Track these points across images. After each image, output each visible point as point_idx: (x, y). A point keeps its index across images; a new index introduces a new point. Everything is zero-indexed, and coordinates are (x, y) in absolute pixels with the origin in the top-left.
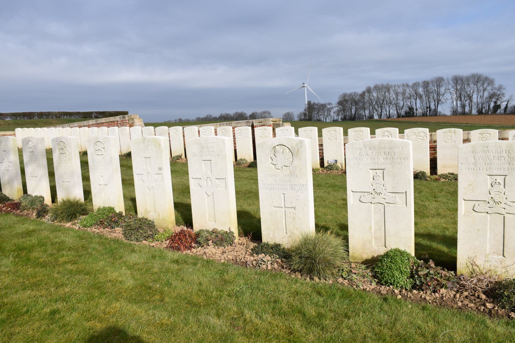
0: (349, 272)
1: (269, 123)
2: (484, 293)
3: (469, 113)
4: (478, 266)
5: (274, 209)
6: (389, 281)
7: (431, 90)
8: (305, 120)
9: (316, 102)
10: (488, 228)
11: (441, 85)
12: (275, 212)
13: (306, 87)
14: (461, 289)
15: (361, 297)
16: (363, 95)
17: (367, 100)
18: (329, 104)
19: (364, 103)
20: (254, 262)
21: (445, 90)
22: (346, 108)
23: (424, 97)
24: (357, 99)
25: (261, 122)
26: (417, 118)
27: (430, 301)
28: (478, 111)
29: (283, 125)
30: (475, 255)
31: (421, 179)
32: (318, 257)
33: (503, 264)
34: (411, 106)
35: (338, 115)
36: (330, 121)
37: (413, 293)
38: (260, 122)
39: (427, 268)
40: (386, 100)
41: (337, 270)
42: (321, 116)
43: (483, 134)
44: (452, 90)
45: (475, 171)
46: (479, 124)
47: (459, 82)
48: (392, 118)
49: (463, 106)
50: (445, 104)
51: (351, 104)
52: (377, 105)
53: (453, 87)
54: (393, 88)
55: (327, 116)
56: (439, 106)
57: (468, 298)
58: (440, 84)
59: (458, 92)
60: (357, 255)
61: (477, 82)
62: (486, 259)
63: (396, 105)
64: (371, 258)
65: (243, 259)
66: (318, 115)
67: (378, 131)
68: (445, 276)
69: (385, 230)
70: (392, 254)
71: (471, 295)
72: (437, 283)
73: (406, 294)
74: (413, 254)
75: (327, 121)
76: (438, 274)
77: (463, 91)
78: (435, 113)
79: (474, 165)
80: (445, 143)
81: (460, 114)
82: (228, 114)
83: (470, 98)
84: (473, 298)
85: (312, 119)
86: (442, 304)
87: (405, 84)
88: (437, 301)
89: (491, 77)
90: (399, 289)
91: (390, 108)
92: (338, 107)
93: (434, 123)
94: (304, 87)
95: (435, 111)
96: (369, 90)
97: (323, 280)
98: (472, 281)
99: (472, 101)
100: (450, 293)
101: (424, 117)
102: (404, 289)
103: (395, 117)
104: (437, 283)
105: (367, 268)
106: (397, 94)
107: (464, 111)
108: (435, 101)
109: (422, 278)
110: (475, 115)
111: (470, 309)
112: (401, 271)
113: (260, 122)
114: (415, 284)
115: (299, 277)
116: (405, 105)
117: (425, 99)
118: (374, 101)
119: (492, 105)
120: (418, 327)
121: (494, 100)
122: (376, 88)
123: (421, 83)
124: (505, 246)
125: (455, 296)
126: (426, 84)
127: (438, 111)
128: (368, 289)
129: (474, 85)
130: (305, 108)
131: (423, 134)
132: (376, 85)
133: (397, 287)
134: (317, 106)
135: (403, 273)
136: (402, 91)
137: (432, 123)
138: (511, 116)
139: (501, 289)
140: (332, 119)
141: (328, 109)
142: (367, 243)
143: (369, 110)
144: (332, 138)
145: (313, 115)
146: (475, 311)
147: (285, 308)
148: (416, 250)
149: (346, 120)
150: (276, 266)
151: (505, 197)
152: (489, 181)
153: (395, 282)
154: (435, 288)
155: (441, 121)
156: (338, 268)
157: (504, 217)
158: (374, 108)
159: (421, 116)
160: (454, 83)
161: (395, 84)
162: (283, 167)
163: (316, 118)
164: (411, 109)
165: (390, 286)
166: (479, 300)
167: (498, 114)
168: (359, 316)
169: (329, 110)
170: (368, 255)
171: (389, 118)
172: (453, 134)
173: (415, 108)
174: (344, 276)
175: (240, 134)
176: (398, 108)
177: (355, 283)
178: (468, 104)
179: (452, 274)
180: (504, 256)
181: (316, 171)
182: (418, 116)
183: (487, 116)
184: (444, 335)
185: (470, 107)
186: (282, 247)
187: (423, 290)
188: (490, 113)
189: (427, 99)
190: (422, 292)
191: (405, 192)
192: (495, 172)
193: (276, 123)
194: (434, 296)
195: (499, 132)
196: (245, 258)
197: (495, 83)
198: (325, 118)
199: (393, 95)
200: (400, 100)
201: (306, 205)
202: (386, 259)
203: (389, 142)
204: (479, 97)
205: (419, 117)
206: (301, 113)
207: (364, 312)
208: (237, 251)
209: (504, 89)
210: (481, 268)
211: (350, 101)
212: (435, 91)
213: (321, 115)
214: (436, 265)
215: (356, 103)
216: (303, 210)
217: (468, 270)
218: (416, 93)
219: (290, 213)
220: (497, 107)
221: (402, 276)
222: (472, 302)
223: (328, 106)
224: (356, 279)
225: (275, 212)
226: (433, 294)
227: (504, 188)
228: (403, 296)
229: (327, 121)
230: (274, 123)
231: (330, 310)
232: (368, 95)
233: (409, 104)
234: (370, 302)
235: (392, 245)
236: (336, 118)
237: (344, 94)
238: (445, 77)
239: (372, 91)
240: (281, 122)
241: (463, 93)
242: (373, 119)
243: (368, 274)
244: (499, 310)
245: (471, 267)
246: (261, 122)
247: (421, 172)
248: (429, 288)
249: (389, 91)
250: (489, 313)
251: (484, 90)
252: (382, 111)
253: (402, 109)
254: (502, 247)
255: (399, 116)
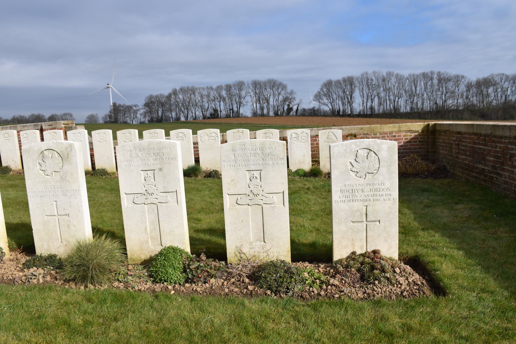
0: (125, 274)
1: (60, 126)
2: (248, 277)
3: (267, 114)
4: (244, 254)
5: (46, 218)
6: (163, 279)
7: (234, 93)
8: (110, 123)
9: (121, 104)
10: (250, 219)
11: (242, 89)
12: (48, 221)
13: (110, 88)
14: (229, 276)
15: (133, 298)
16: (169, 97)
17: (173, 102)
18: (135, 106)
19: (171, 105)
20: (23, 278)
21: (246, 93)
22: (153, 110)
23: (227, 99)
24: (163, 101)
25: (51, 125)
26: (221, 119)
27: (201, 292)
28: (274, 113)
29: (76, 128)
30: (241, 244)
31: (214, 177)
32: (91, 263)
33: (264, 249)
34: (216, 108)
35: (145, 117)
36: (136, 123)
37: (185, 286)
38: (49, 125)
39: (199, 261)
40: (192, 103)
41: (113, 274)
42: (127, 118)
43: (266, 134)
44: (252, 93)
45: (236, 167)
46: (275, 125)
47: (258, 86)
48: (198, 119)
49: (262, 109)
50: (246, 106)
51: (158, 106)
52: (184, 107)
53: (252, 91)
54: (198, 90)
55: (133, 118)
56: (241, 108)
57: (234, 284)
58: (241, 88)
59: (257, 95)
60: (135, 256)
61: (273, 87)
62: (251, 247)
63: (202, 107)
64: (149, 258)
65: (10, 276)
66: (124, 117)
67: (172, 133)
68: (215, 266)
69: (160, 229)
70: (165, 252)
71: (238, 281)
72: (207, 274)
73: (179, 289)
74: (188, 249)
75: (134, 123)
76: (208, 265)
77: (261, 95)
78: (238, 115)
79: (234, 162)
80: (124, 143)
81: (259, 116)
82: (23, 117)
83: (268, 101)
84: (238, 283)
85: (118, 122)
86: (211, 293)
87: (209, 86)
88: (207, 291)
89: (284, 83)
90: (173, 285)
91: (196, 110)
92: (144, 109)
93: (237, 124)
94: (108, 87)
95: (238, 113)
96: (175, 92)
97: (99, 286)
98: (238, 267)
99: (269, 104)
100: (219, 282)
101: (227, 119)
102: (178, 284)
103: (201, 118)
104: (207, 274)
105: (144, 268)
106: (202, 97)
107: (263, 112)
108: (237, 103)
109: (194, 272)
110: (273, 116)
111: (235, 293)
112: (174, 267)
113: (49, 125)
114: (188, 278)
115: (73, 286)
116: (209, 107)
117: (228, 102)
118: (180, 102)
119: (286, 107)
120: (183, 318)
121: (287, 103)
122: (182, 90)
123: (224, 86)
124: (265, 233)
125: (223, 283)
126: (228, 88)
127: (240, 113)
128: (143, 289)
129: (271, 89)
130: (109, 110)
131: (214, 135)
132: (182, 87)
133: (171, 282)
134: (123, 107)
135: (176, 269)
136: (206, 93)
137: (235, 124)
138: (301, 117)
139: (259, 271)
140: (139, 121)
141: (134, 111)
142: (144, 243)
143: (176, 112)
144: (127, 141)
145: (119, 117)
146: (239, 294)
147: (50, 321)
148: (191, 244)
149: (153, 122)
150: (48, 278)
151: (261, 189)
152: (248, 176)
153: (169, 278)
154: (206, 279)
155: (243, 123)
156: (115, 272)
157: (262, 207)
158: (180, 110)
159: (225, 118)
160: (254, 87)
161: (200, 86)
162: (53, 172)
163: (122, 121)
164: (216, 111)
165: (165, 283)
166: (243, 284)
167: (291, 116)
168: (128, 317)
169: (135, 112)
170: (145, 256)
171: (195, 119)
172: (241, 134)
173: (219, 110)
174: (120, 280)
175: (27, 139)
176: (203, 110)
177: (130, 285)
178: (266, 107)
179: (222, 264)
180: (265, 242)
181: (111, 174)
182: (222, 117)
183: (282, 117)
184: (207, 321)
185: (267, 109)
186: (58, 257)
187: (195, 283)
188: (284, 114)
189: (230, 101)
190: (194, 285)
191: (282, 192)
192: (252, 168)
193: (68, 125)
194: (205, 287)
195: (280, 132)
196: (13, 274)
197: (288, 88)
198: (131, 120)
199: (198, 98)
200: (205, 102)
201: (80, 211)
202: (159, 257)
203: (158, 143)
204: (275, 100)
205: (223, 118)
206: (106, 115)
207: (134, 313)
208: (5, 268)
209: (295, 93)
210: (247, 255)
211: (156, 103)
212: (237, 94)
213: (127, 117)
214: (208, 257)
215: (163, 105)
216: (78, 216)
217: (237, 258)
218: (220, 96)
219: (64, 221)
220: (290, 109)
221: (175, 272)
222: (238, 287)
223: (134, 108)
224: (132, 280)
225: (48, 221)
226: (204, 285)
227: (261, 181)
228: (176, 291)
229: (134, 123)
230: (66, 126)
231: (99, 316)
232: (175, 97)
233: (214, 106)
234: (141, 302)
235: (168, 243)
236: (142, 120)
237: (150, 95)
238: (245, 82)
239: (178, 93)
240: (74, 125)
241: (262, 97)
242: (180, 121)
243: (144, 274)
244: (258, 291)
245: (239, 255)
246: (51, 125)
247: (214, 171)
248: (200, 280)
249: (194, 93)
250: (250, 294)
251: (279, 94)
252: (188, 113)
253: (207, 111)
254: (263, 235)
255: (204, 117)
